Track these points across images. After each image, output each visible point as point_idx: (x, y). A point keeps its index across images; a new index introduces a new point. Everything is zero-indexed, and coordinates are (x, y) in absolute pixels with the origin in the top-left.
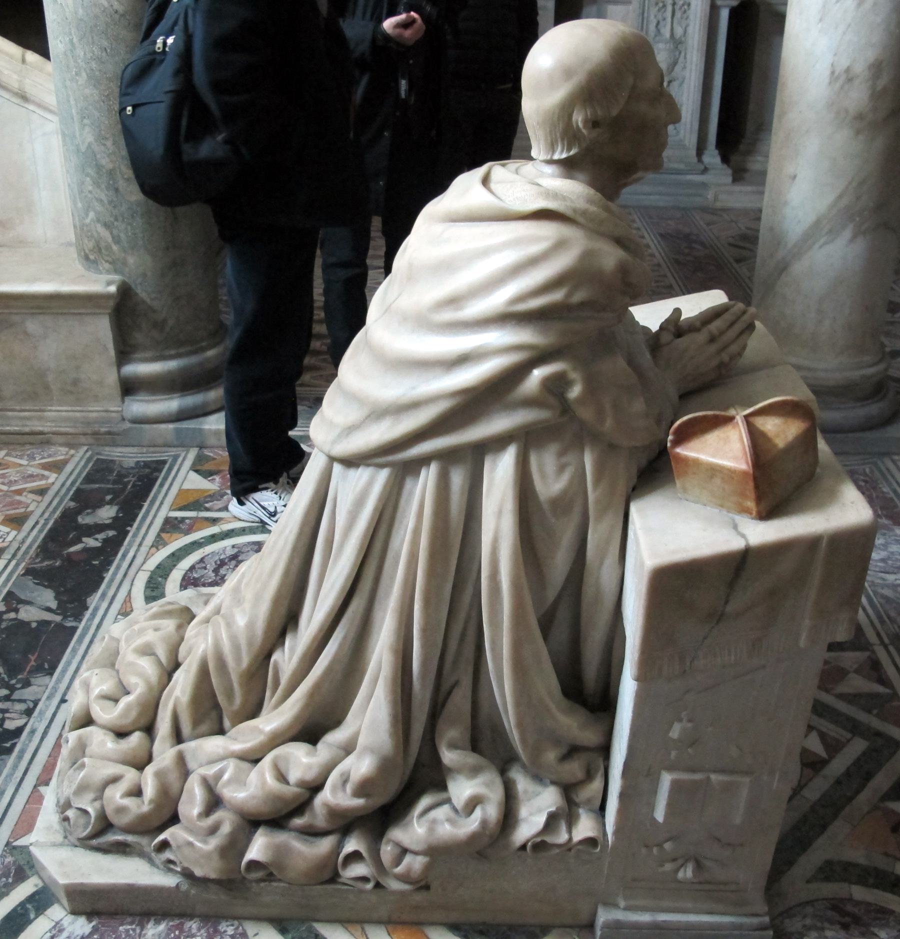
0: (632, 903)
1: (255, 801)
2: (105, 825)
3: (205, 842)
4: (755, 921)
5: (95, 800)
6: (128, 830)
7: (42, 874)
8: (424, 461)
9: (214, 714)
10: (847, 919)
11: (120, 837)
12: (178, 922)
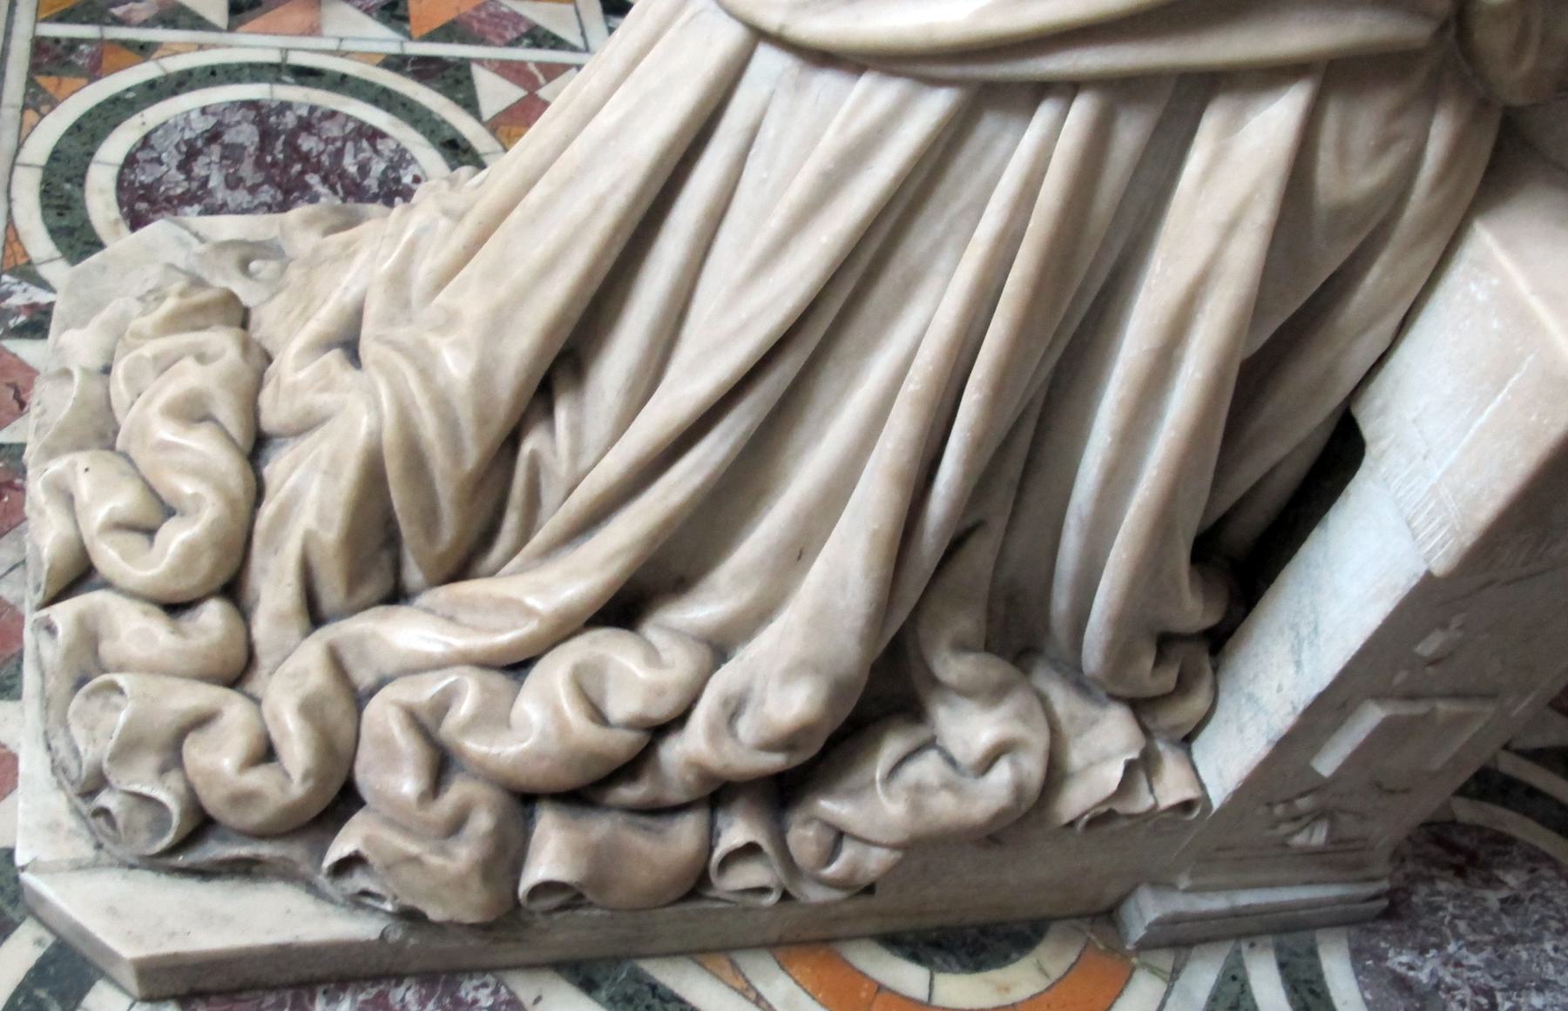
0: (1202, 881)
1: (545, 764)
2: (201, 825)
3: (443, 852)
4: (1371, 889)
5: (163, 771)
6: (260, 835)
7: (40, 912)
8: (1068, 88)
9: (385, 558)
10: (1460, 859)
11: (244, 850)
12: (374, 991)
